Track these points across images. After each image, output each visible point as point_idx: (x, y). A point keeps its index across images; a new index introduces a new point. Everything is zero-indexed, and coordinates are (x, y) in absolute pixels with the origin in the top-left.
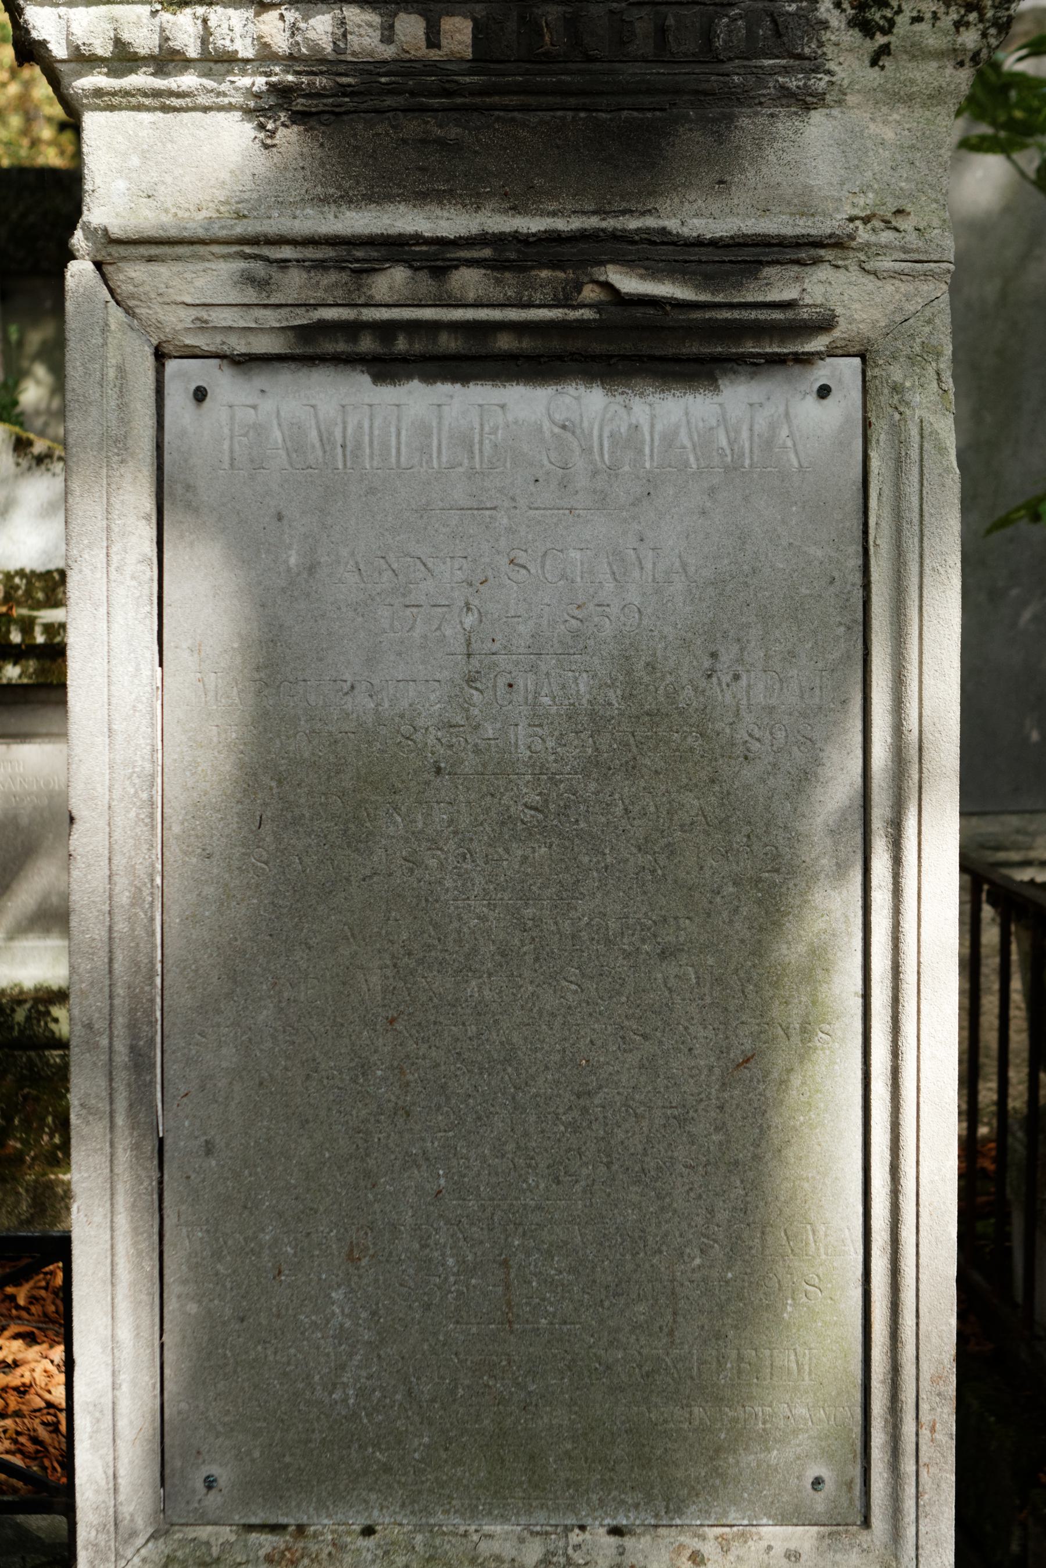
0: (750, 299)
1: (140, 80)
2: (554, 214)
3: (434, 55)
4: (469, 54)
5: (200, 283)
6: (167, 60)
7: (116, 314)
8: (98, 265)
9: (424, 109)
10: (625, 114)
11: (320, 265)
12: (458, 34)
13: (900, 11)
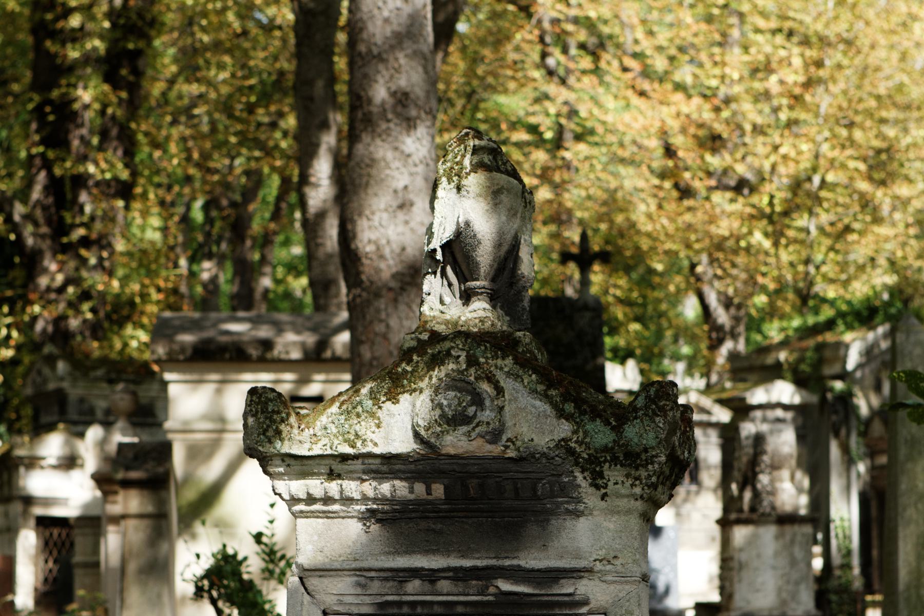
0: (555, 592)
1: (318, 507)
2: (478, 558)
3: (430, 497)
4: (443, 497)
5: (339, 586)
6: (327, 500)
7: (307, 598)
8: (301, 578)
9: (428, 518)
10: (506, 519)
11: (386, 579)
12: (438, 490)
13: (609, 480)
